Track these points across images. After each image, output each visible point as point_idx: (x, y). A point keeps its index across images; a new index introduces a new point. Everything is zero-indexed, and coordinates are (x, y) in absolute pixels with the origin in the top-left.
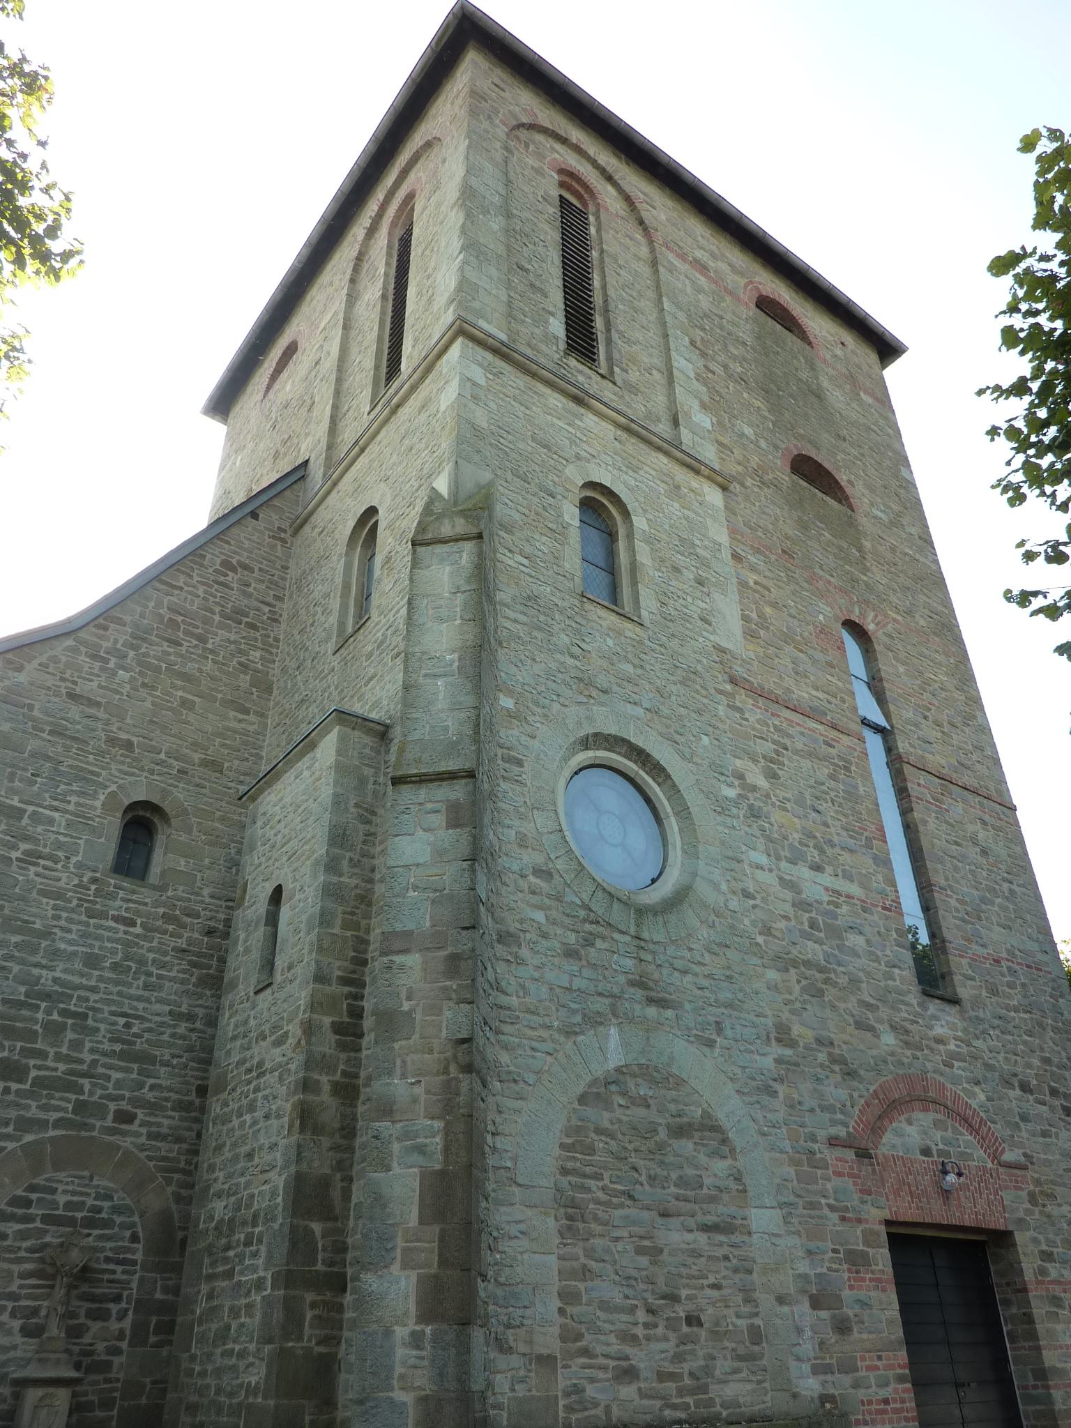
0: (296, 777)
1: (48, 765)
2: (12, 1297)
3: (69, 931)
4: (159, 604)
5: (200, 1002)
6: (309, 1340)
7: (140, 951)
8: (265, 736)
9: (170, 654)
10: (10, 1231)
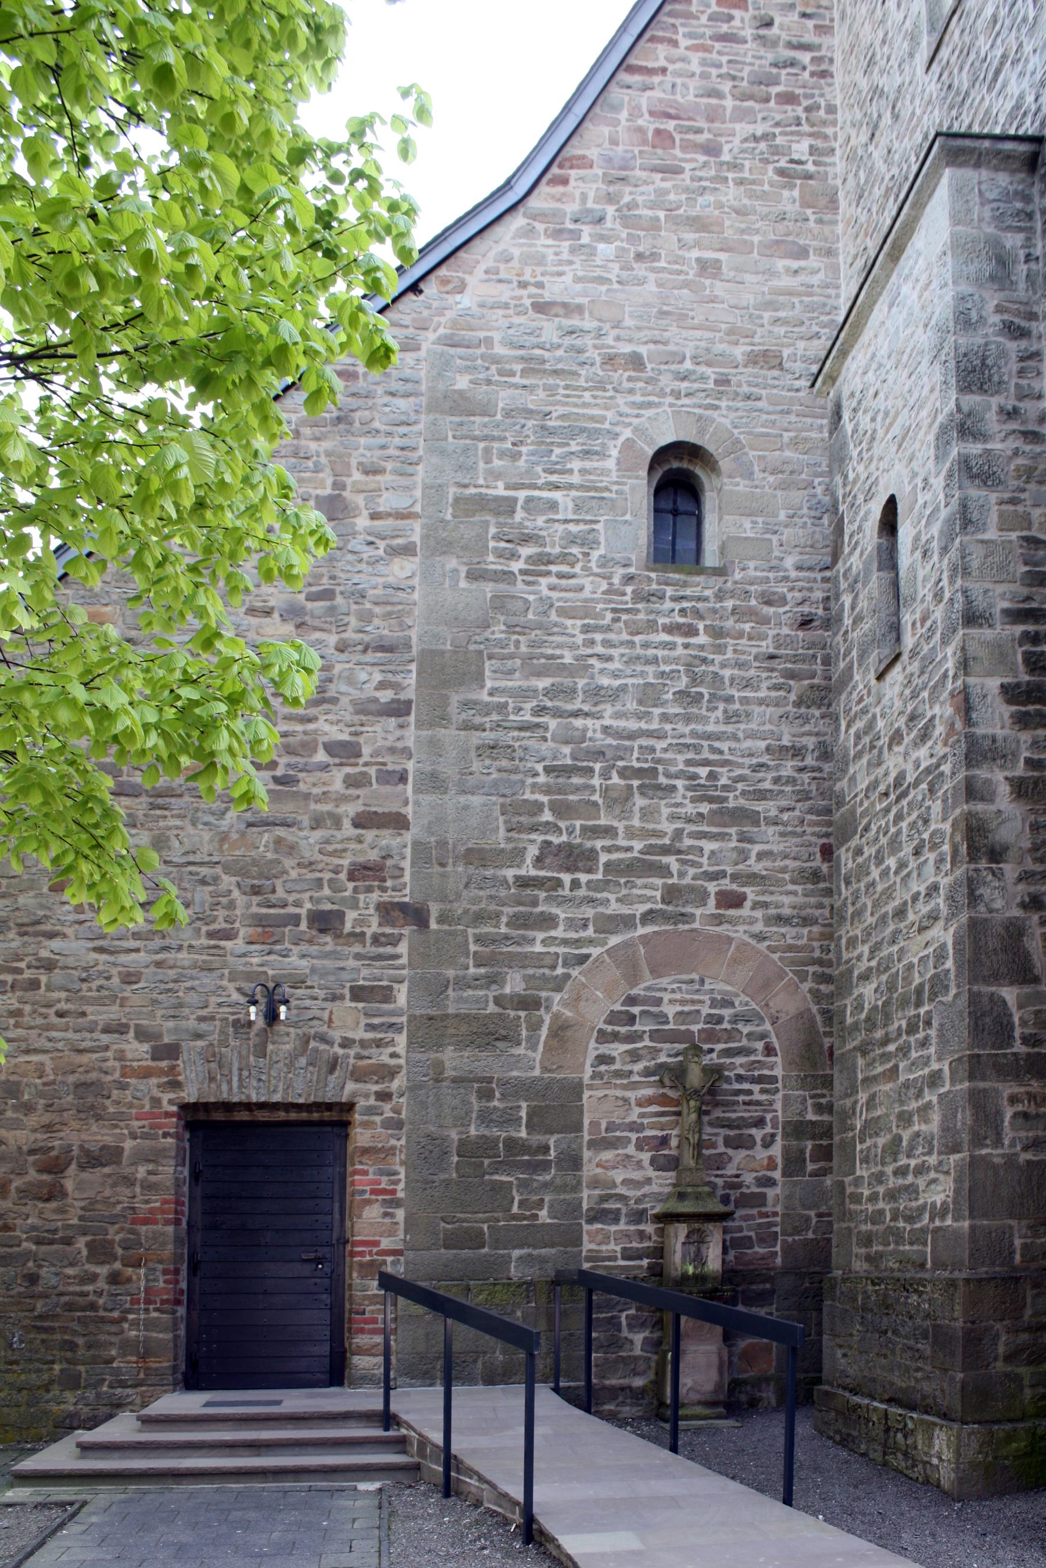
0: (891, 306)
1: (530, 423)
2: (634, 1127)
3: (609, 659)
4: (635, 113)
5: (807, 728)
6: (1012, 1145)
7: (711, 669)
8: (838, 287)
9: (667, 192)
10: (615, 1054)
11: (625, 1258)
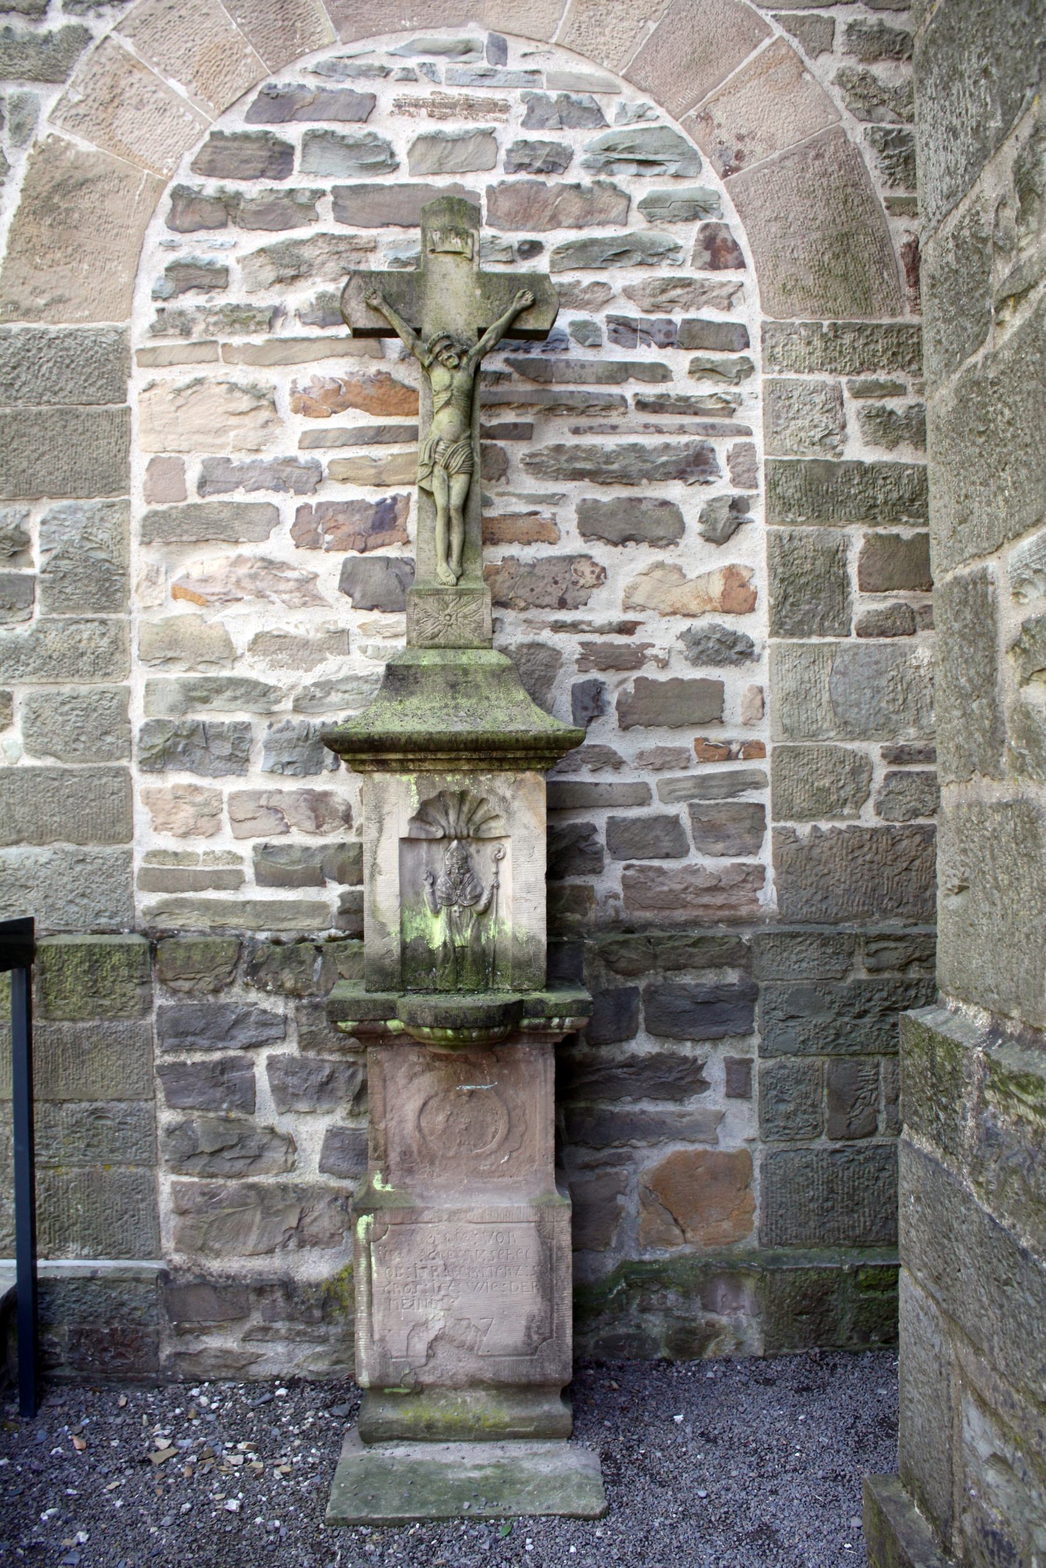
10: (225, 259)
11: (267, 878)
